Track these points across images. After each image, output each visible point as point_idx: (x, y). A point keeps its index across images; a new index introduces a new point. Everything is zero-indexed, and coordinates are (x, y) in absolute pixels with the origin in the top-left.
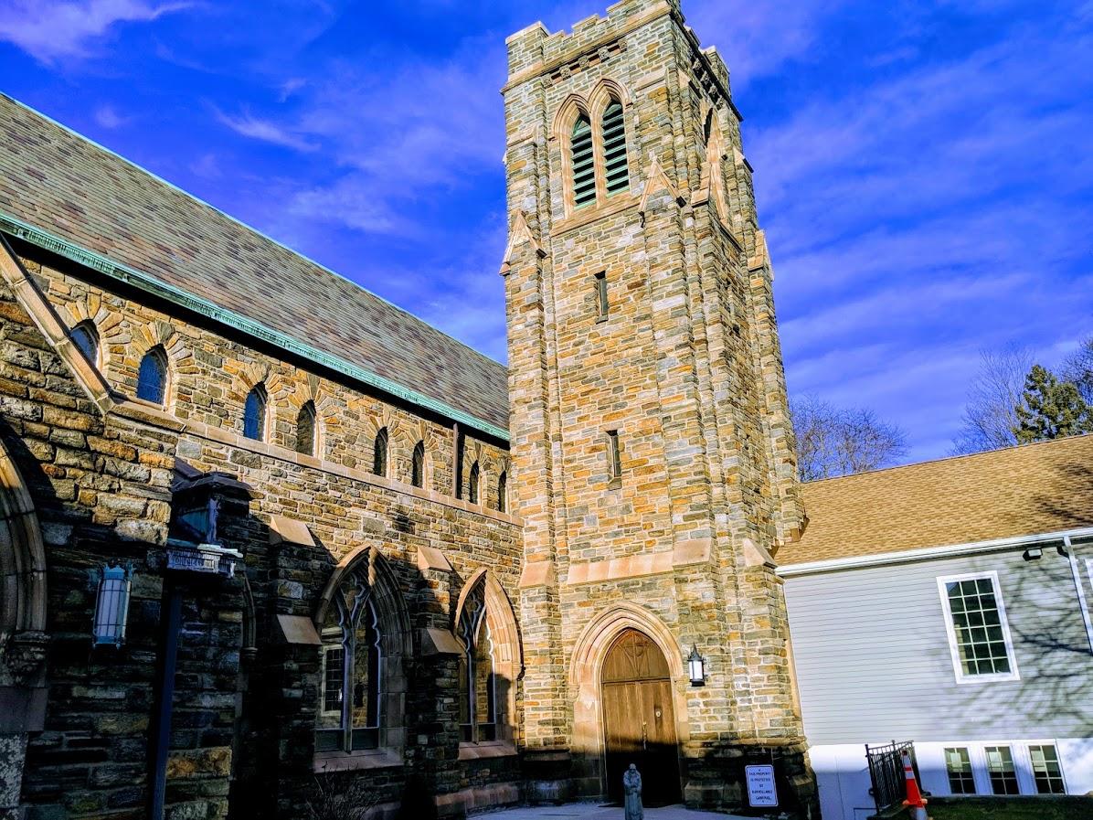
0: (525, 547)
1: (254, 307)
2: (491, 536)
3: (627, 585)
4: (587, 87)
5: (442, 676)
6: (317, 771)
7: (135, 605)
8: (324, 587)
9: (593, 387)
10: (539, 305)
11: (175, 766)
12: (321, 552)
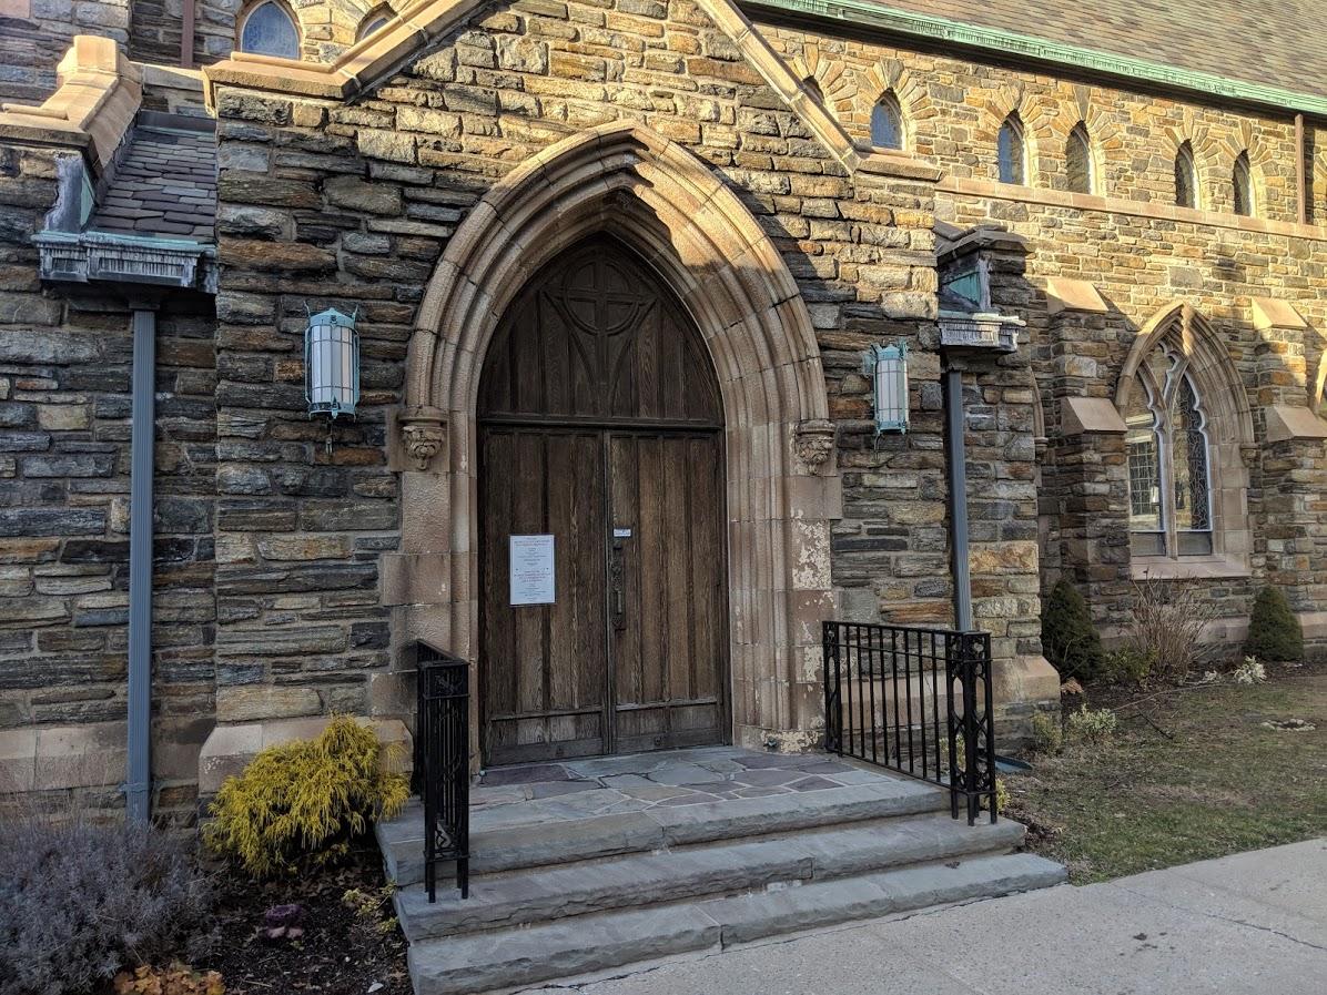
1: (994, 11)
5: (1301, 466)
6: (1137, 578)
8: (1123, 361)
11: (977, 559)
12: (1114, 318)
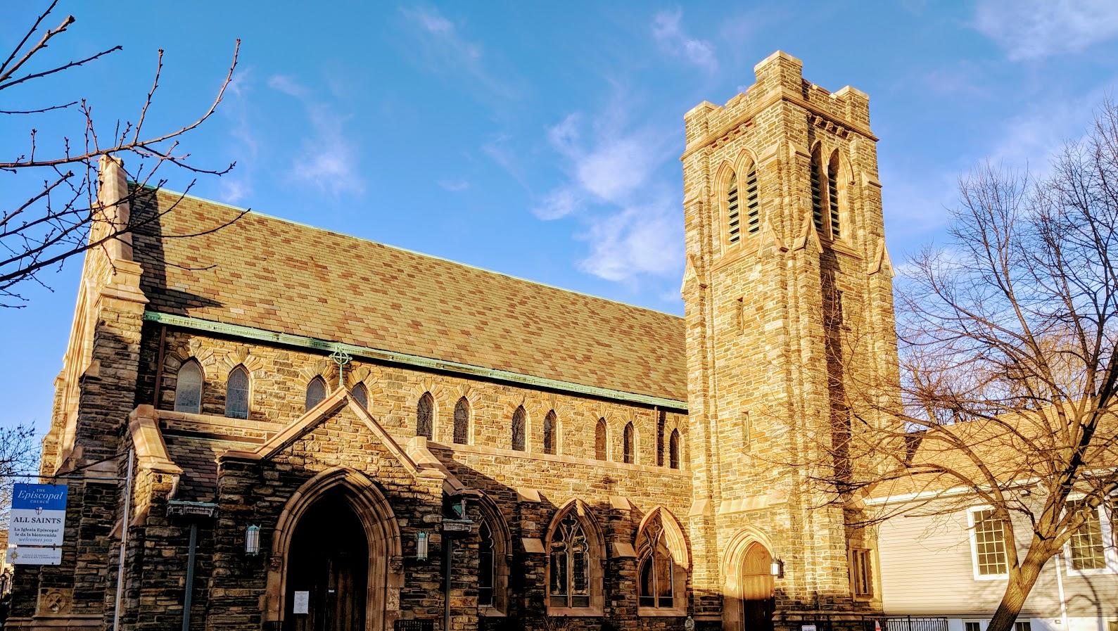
0: (694, 490)
2: (665, 485)
3: (752, 515)
4: (734, 154)
5: (623, 569)
7: (430, 545)
8: (549, 523)
9: (735, 381)
10: (702, 324)
12: (544, 502)
